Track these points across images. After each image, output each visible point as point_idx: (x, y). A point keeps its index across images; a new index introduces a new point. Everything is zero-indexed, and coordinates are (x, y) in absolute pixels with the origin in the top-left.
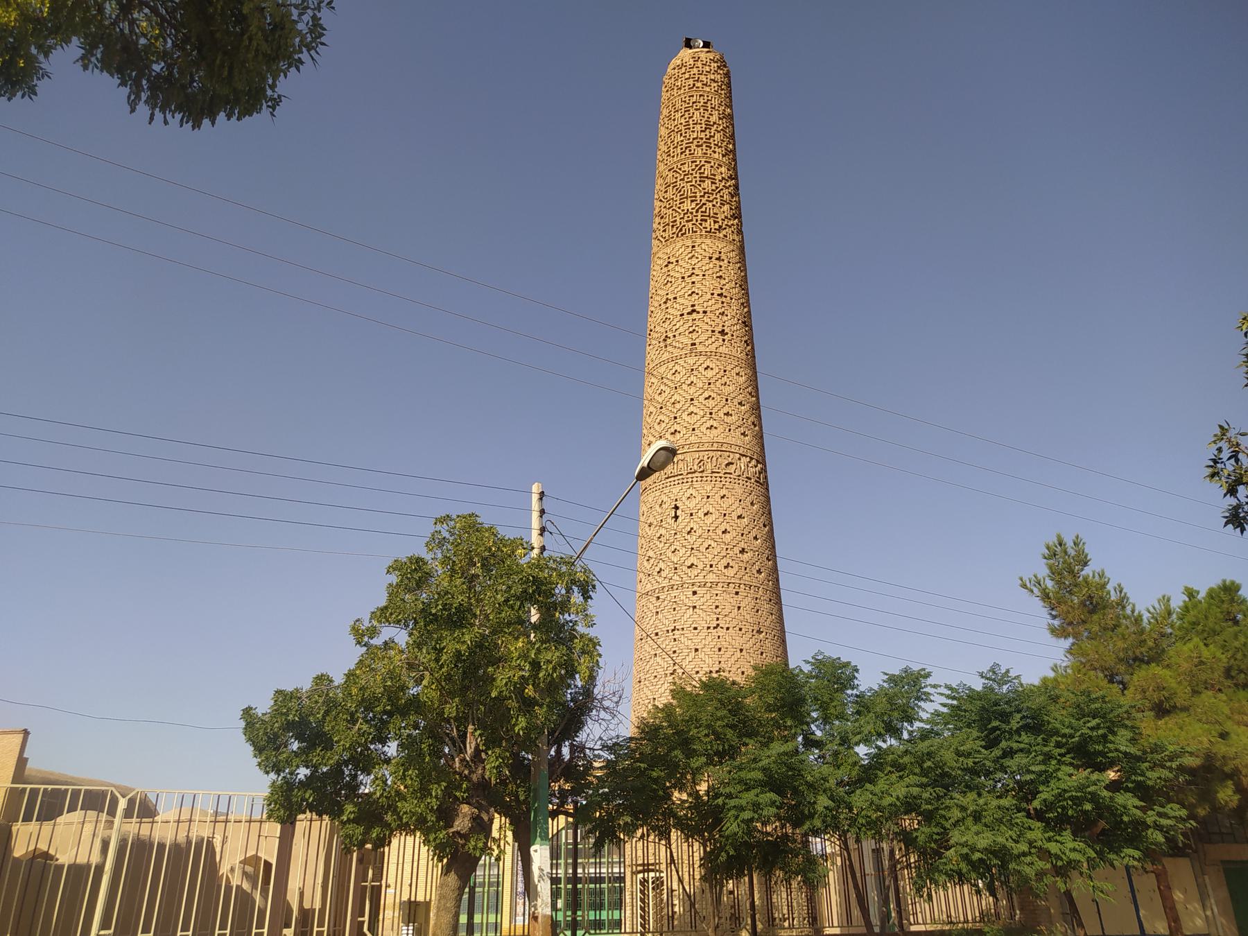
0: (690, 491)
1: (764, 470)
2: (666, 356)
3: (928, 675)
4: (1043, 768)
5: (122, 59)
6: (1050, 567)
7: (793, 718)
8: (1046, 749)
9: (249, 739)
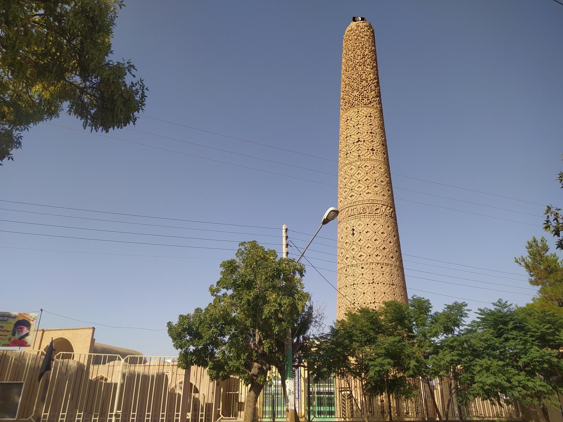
0: (360, 222)
1: (394, 211)
2: (347, 162)
3: (466, 305)
4: (522, 347)
5: (80, 110)
6: (529, 252)
7: (401, 325)
8: (524, 338)
9: (170, 335)
